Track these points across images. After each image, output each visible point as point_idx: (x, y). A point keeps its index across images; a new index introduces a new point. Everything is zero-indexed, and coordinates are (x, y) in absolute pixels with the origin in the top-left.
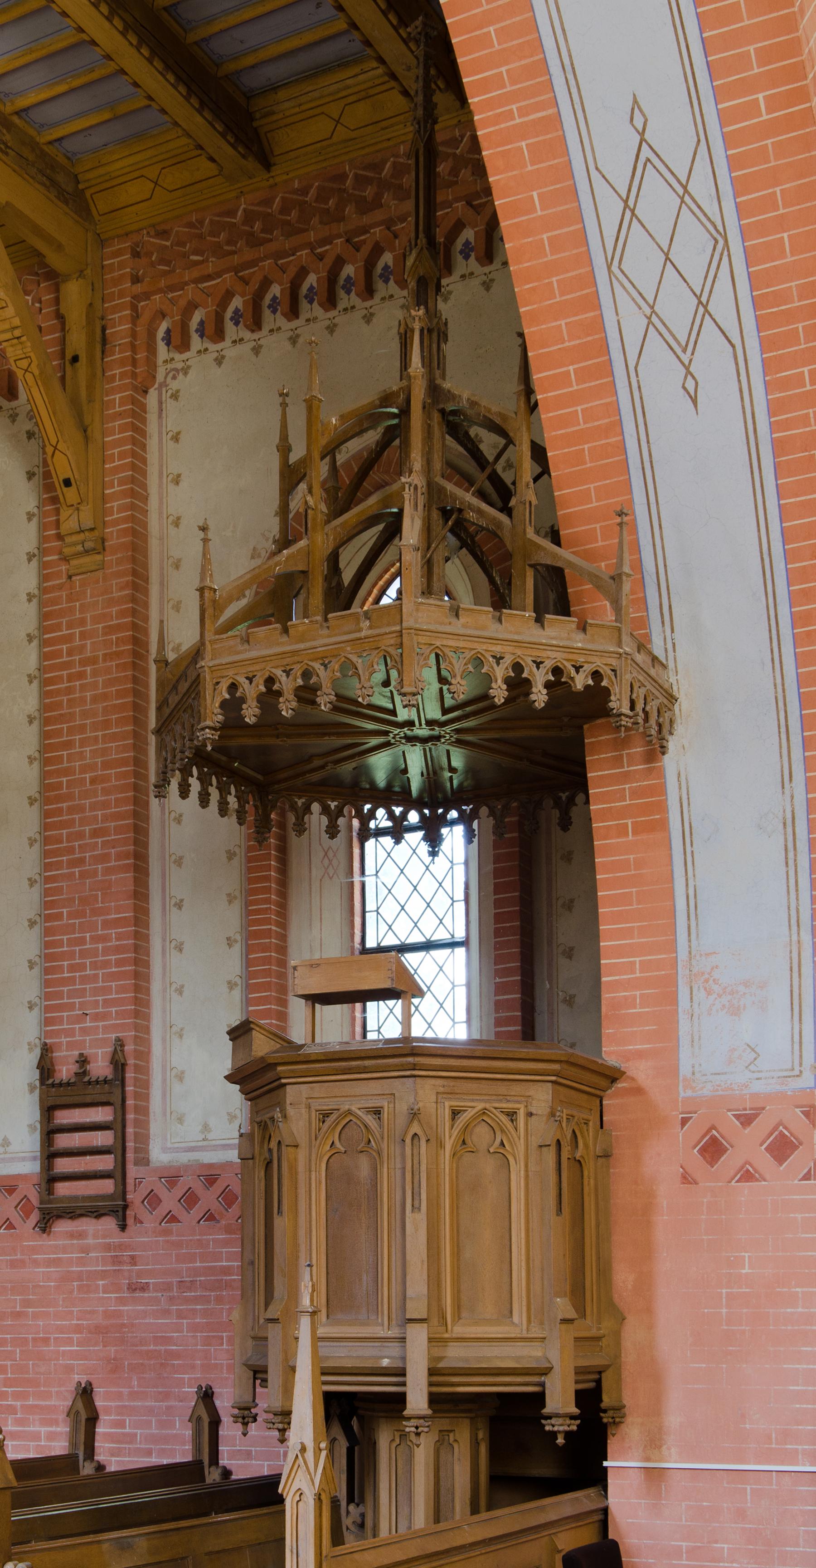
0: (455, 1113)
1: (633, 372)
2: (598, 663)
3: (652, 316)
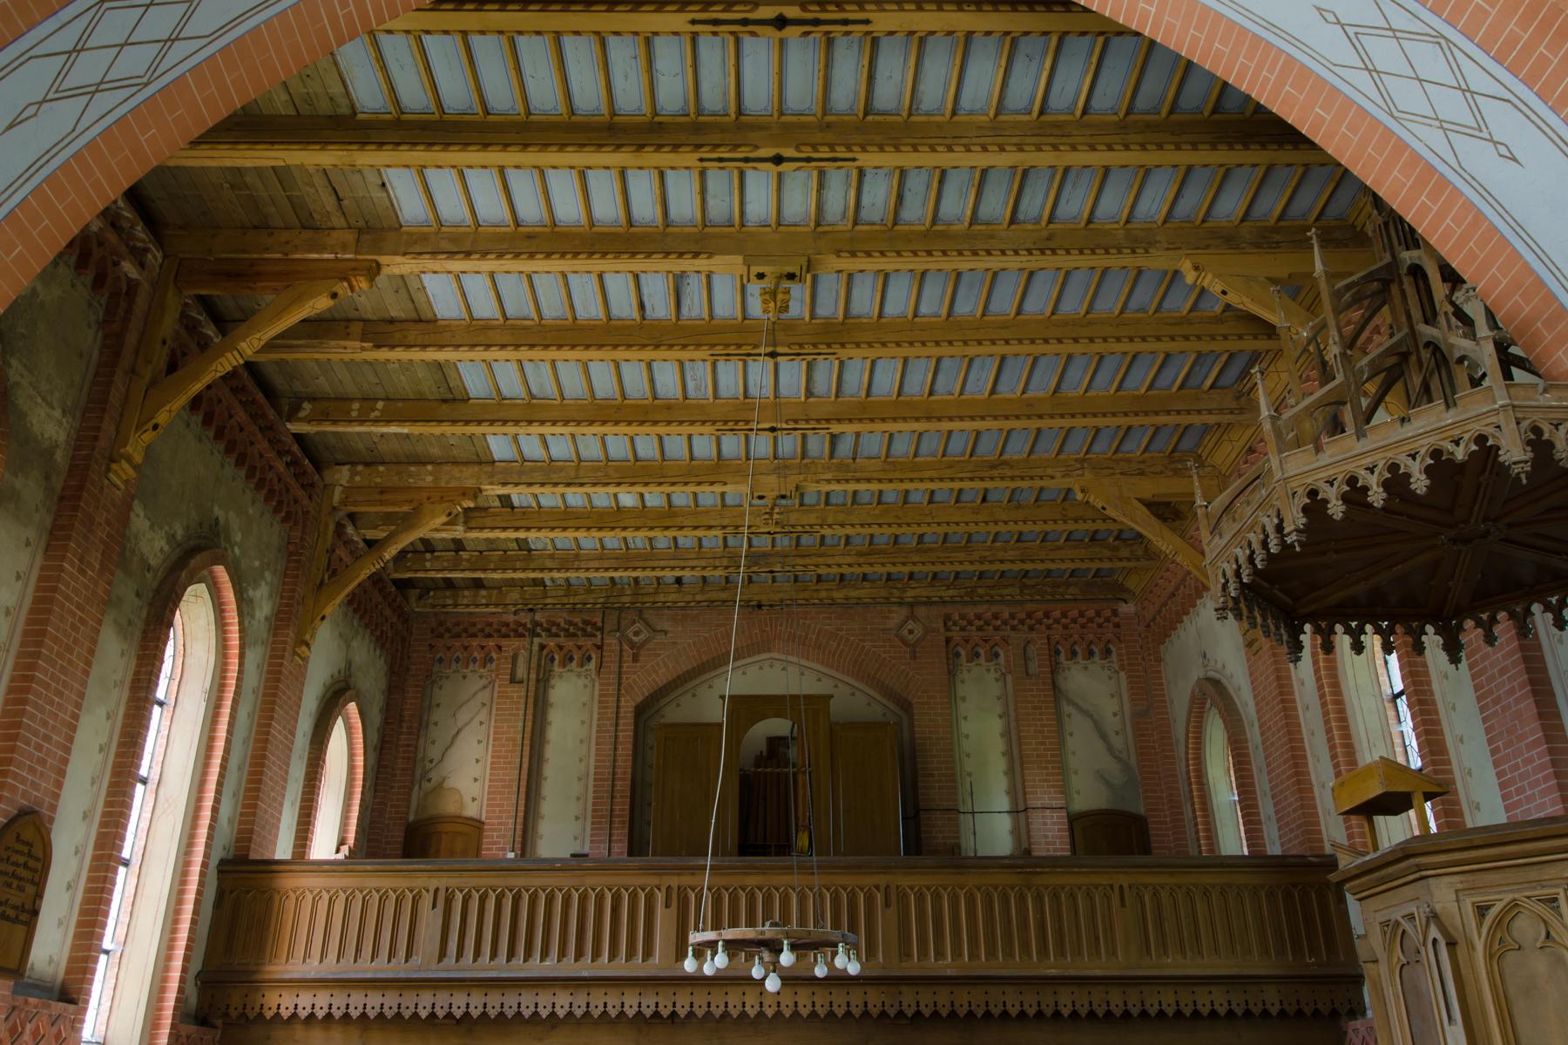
0: (1482, 911)
1: (1460, 170)
2: (1477, 428)
3: (1443, 125)
